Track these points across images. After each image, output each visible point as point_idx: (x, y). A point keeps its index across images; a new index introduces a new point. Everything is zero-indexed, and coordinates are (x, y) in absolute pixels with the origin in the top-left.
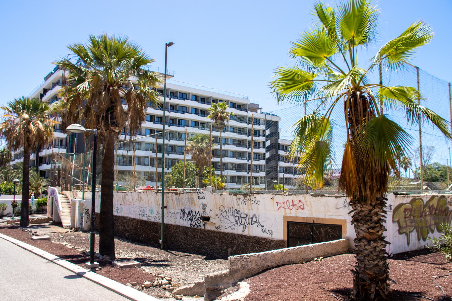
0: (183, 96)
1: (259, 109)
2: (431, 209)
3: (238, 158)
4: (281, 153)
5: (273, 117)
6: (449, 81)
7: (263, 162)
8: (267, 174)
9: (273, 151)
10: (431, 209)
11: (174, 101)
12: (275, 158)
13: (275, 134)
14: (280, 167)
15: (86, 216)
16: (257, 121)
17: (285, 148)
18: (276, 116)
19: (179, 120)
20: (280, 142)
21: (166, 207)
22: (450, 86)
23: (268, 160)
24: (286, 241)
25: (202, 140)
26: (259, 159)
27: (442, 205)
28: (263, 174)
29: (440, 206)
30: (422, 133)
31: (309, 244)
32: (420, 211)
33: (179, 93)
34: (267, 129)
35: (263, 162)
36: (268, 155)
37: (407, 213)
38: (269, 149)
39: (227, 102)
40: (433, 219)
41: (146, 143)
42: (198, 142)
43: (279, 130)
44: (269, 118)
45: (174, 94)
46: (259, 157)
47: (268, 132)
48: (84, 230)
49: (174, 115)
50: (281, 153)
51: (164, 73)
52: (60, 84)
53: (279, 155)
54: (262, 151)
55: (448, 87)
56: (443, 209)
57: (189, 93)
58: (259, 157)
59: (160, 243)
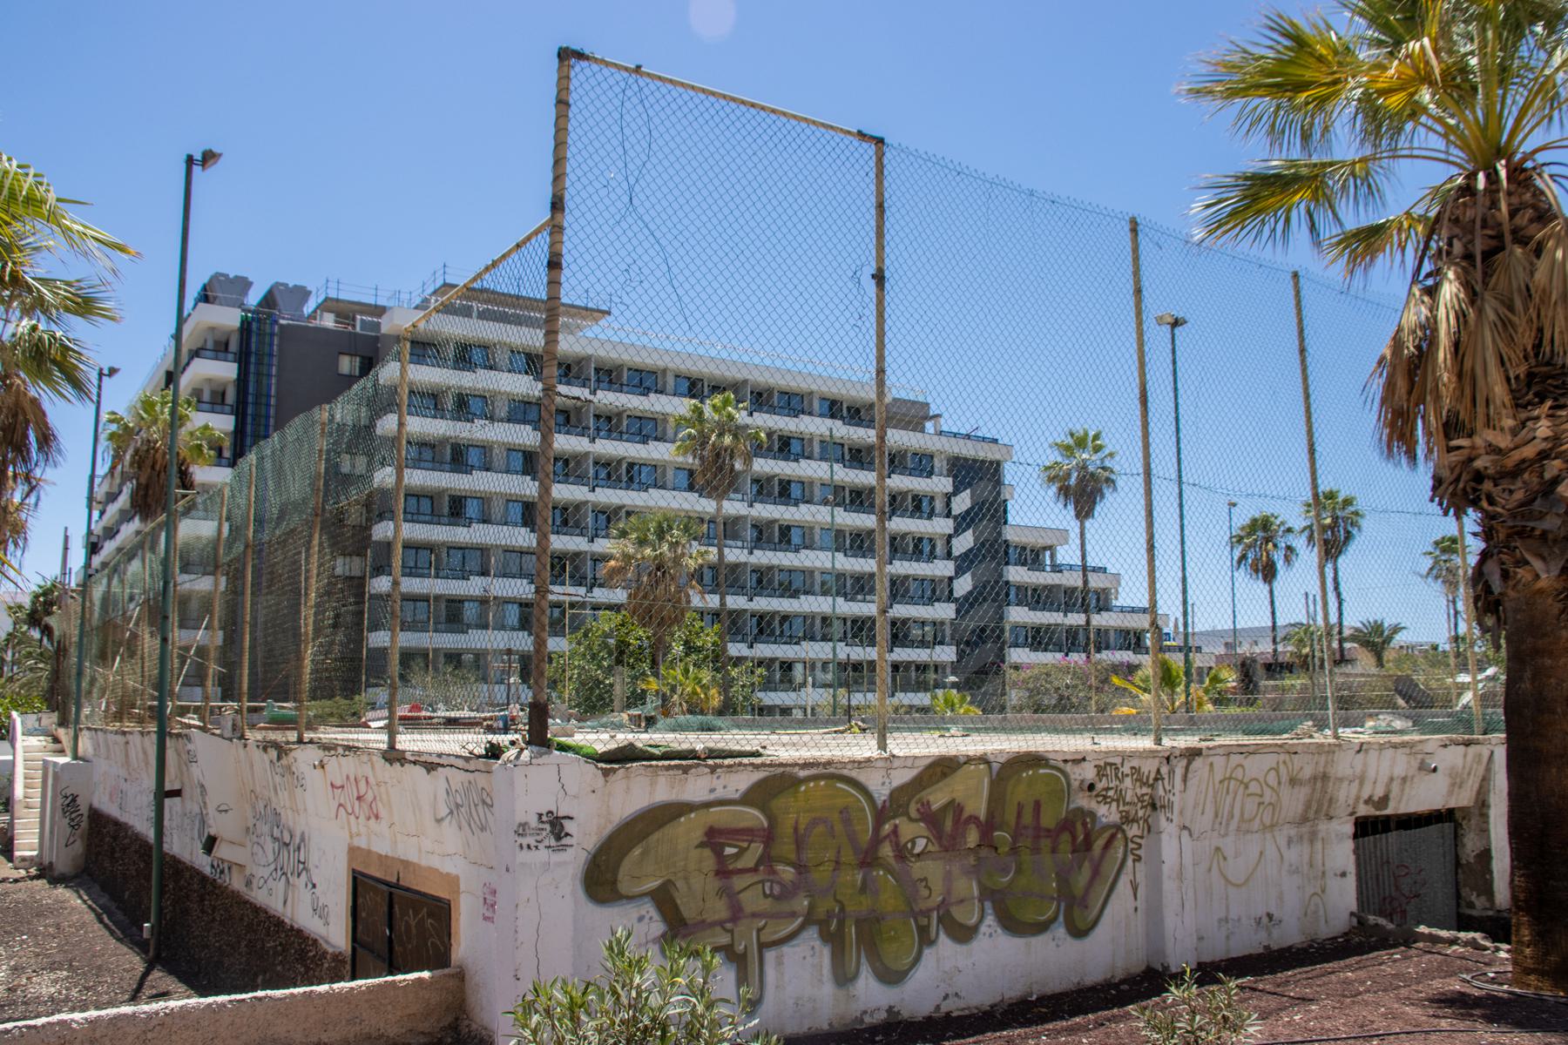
0: (645, 380)
1: (928, 418)
2: (948, 824)
3: (849, 597)
4: (1017, 574)
5: (979, 445)
6: (1134, 211)
7: (944, 611)
8: (961, 654)
9: (983, 568)
10: (948, 824)
11: (608, 399)
12: (994, 593)
13: (991, 511)
14: (1015, 627)
15: (67, 820)
16: (922, 464)
17: (1032, 557)
18: (995, 441)
19: (631, 465)
20: (1010, 534)
21: (177, 793)
22: (1134, 230)
23: (966, 605)
24: (349, 959)
25: (661, 534)
26: (932, 599)
27: (1037, 805)
28: (947, 654)
29: (1020, 807)
30: (1174, 476)
31: (182, 1007)
32: (852, 839)
33: (630, 369)
34: (957, 491)
35: (944, 611)
36: (964, 585)
37: (729, 851)
38: (965, 563)
39: (737, 387)
40: (975, 871)
41: (508, 550)
42: (642, 542)
43: (1005, 494)
44: (967, 450)
45: (609, 375)
46: (935, 591)
47: (962, 503)
48: (56, 873)
49: (608, 447)
50: (1017, 574)
51: (542, 294)
52: (208, 353)
53: (1007, 583)
54: (943, 568)
55: (1128, 236)
56: (1048, 820)
57: (664, 371)
58: (935, 591)
59: (146, 935)
